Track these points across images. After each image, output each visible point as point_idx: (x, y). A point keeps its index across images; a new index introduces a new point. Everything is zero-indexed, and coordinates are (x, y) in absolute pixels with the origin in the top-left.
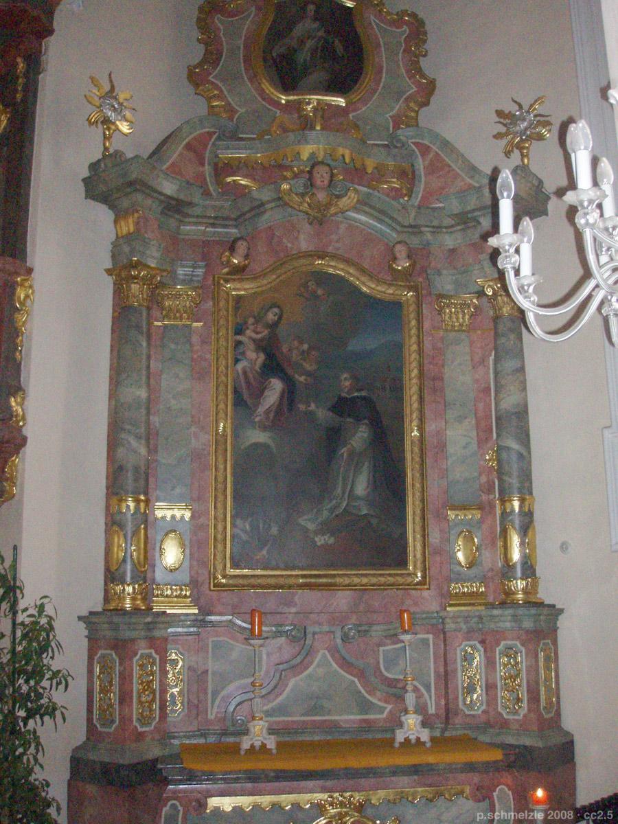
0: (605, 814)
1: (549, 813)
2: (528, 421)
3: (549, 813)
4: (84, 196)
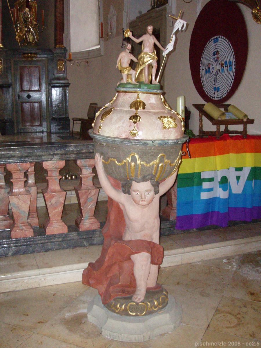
0: (256, 343)
1: (229, 343)
2: (196, 108)
3: (229, 343)
4: (237, 175)
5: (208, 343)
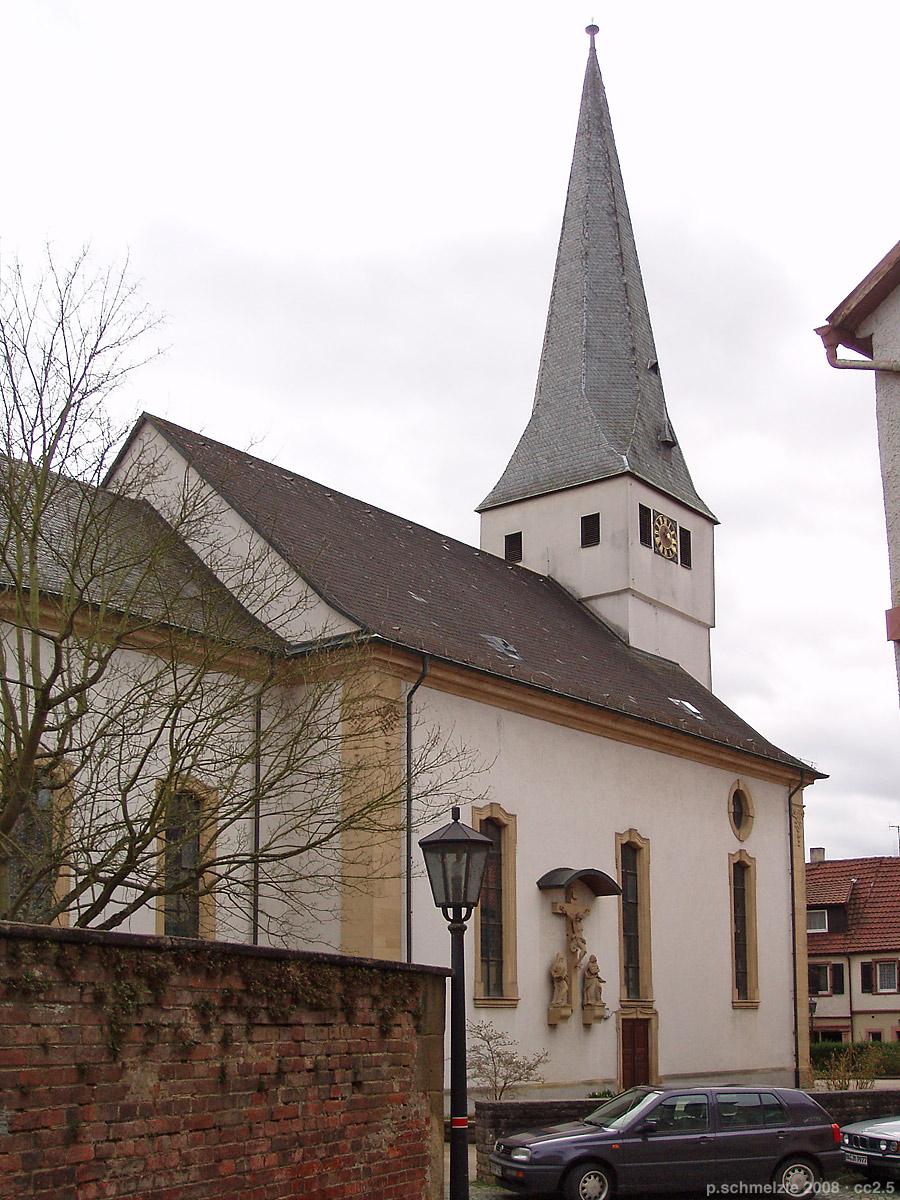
5: (745, 1186)
